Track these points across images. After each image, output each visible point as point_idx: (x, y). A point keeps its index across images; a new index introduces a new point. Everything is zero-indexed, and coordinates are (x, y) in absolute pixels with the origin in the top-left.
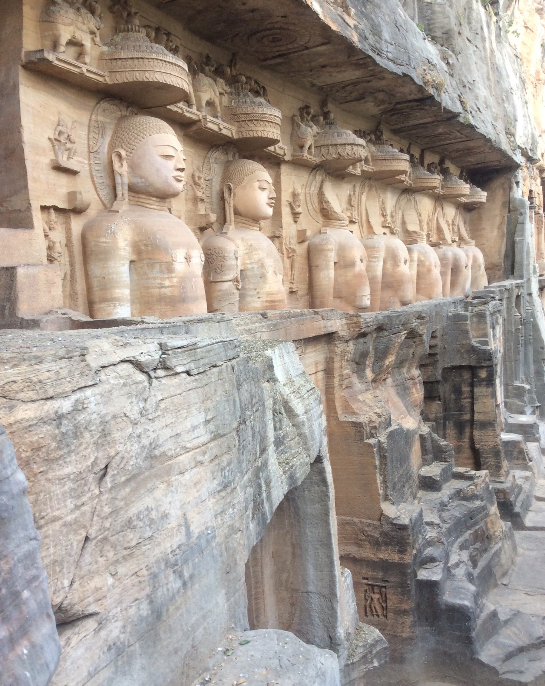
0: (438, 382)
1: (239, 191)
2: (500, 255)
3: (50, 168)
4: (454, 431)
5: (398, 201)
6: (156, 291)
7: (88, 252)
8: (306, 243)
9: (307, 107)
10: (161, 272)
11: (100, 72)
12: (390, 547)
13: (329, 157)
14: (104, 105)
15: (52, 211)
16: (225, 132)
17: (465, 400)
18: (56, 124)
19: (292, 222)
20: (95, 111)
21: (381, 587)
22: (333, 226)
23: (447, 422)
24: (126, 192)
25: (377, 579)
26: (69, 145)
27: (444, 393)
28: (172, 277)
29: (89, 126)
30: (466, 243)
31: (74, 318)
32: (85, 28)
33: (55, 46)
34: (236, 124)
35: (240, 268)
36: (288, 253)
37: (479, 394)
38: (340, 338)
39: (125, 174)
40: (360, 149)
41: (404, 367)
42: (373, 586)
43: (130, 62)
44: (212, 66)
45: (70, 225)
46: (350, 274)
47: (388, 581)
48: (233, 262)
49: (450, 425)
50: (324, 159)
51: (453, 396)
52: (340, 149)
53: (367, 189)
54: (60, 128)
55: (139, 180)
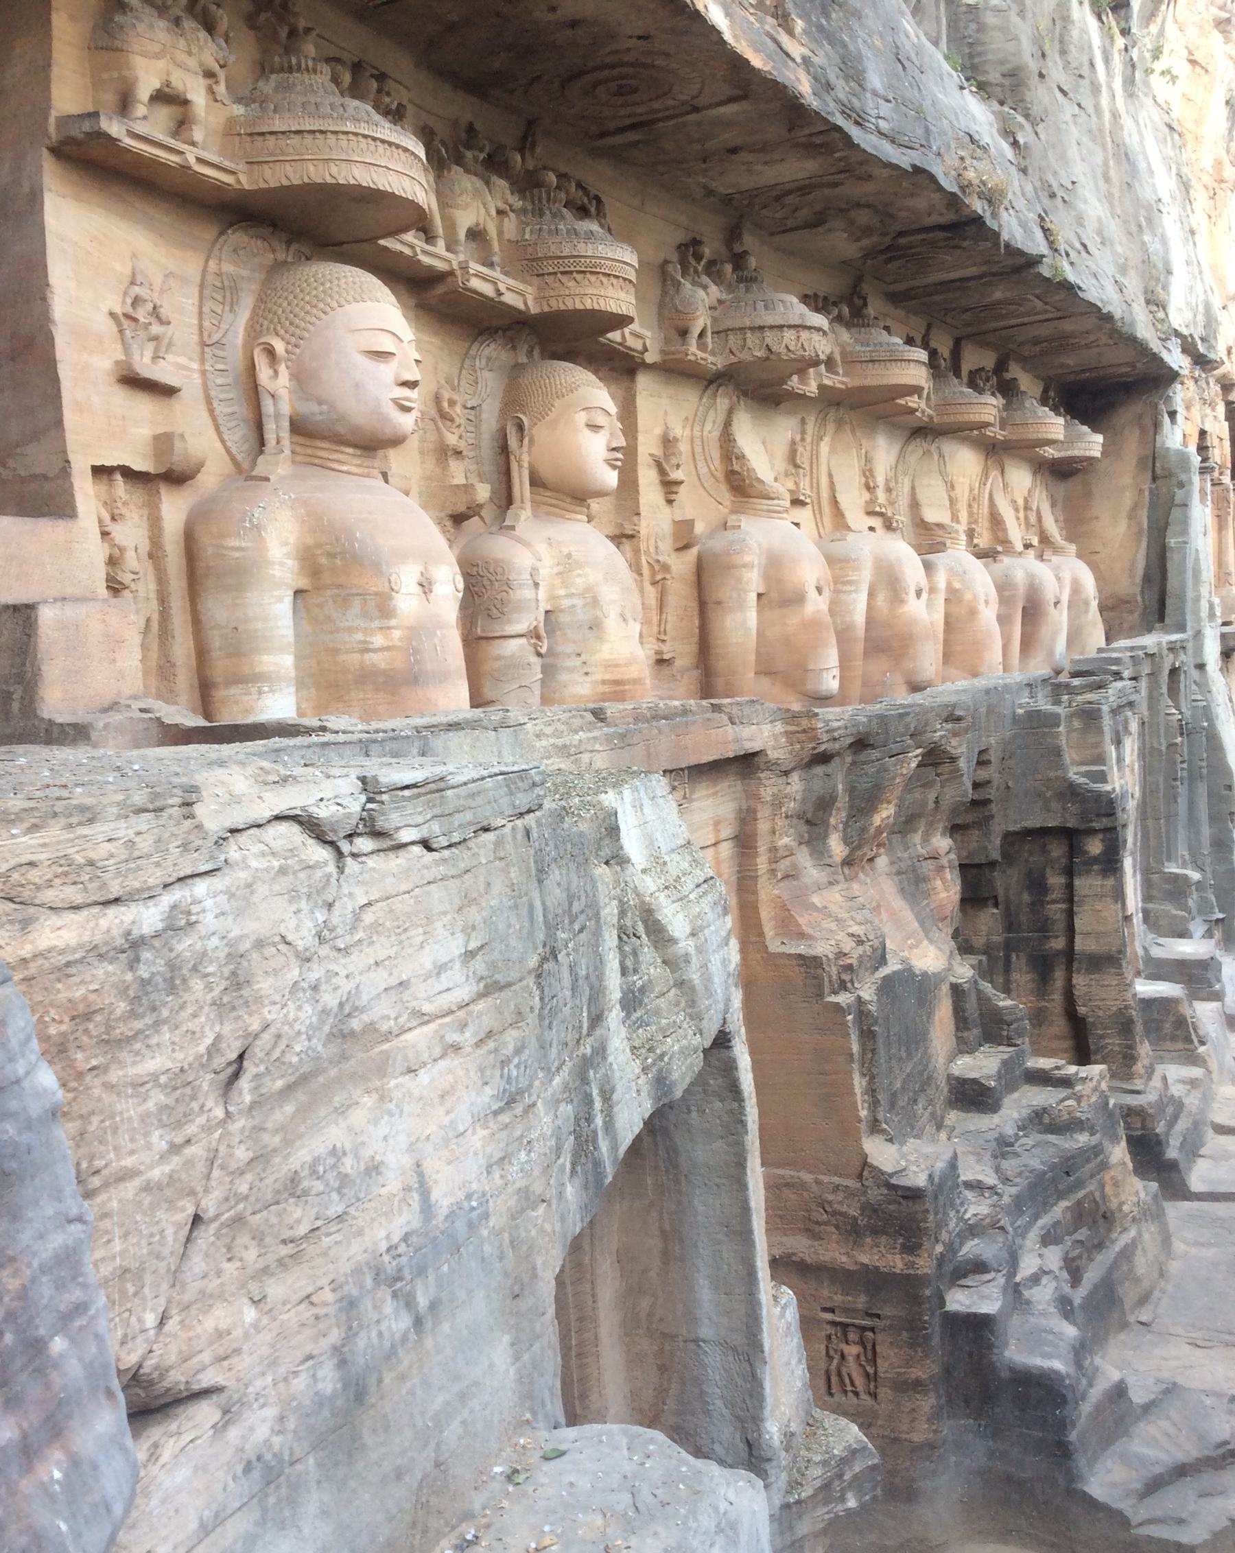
0: (992, 864)
1: (541, 433)
2: (1132, 576)
3: (113, 380)
4: (1029, 977)
5: (902, 454)
6: (353, 659)
7: (199, 572)
8: (694, 551)
9: (696, 242)
10: (365, 615)
11: (227, 164)
12: (883, 1239)
13: (745, 356)
14: (237, 237)
15: (118, 477)
16: (509, 299)
17: (1053, 906)
18: (127, 280)
19: (662, 502)
20: (216, 251)
21: (863, 1329)
22: (755, 512)
23: (1014, 956)
24: (285, 434)
25: (855, 1310)
26: (156, 329)
27: (1007, 889)
28: (389, 628)
29: (202, 286)
30: (1057, 550)
31: (167, 721)
32: (192, 62)
33: (124, 104)
34: (536, 280)
35: (544, 606)
36: (653, 572)
37: (1086, 892)
38: (771, 766)
39: (283, 393)
40: (816, 337)
41: (915, 831)
42: (845, 1326)
43: (295, 141)
44: (481, 151)
45: (159, 510)
46: (792, 621)
47: (878, 1316)
48: (528, 594)
49: (1019, 961)
50: (733, 359)
51: (1026, 897)
52: (770, 337)
53: (831, 427)
54: (136, 290)
55: (315, 408)
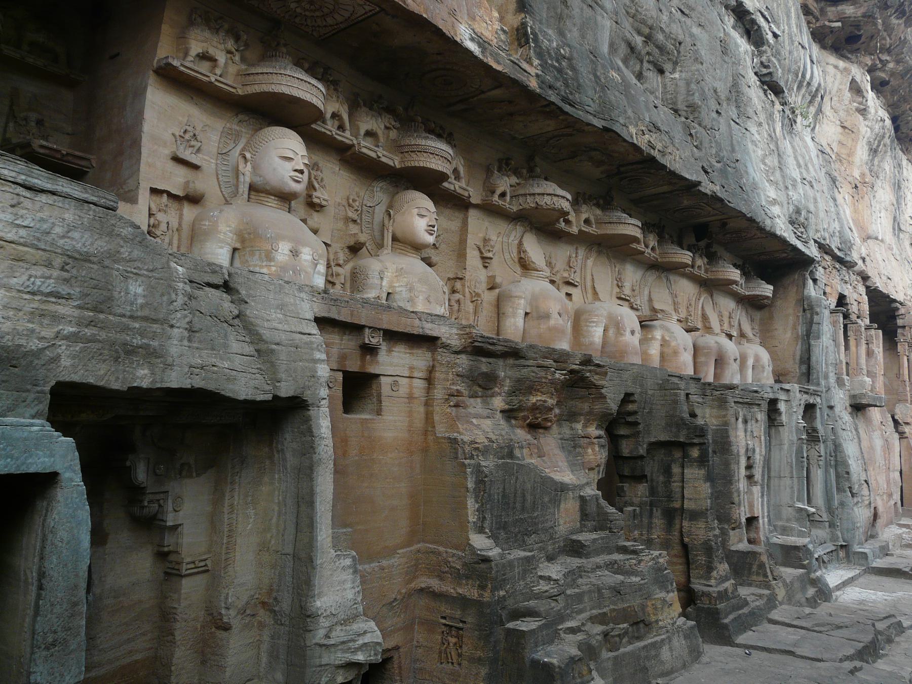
0: (642, 457)
1: (398, 218)
2: (794, 359)
4: (662, 521)
5: (643, 276)
8: (497, 291)
9: (508, 159)
10: (260, 259)
11: (235, 85)
12: (470, 582)
13: (526, 206)
15: (165, 195)
16: (384, 159)
17: (675, 484)
22: (532, 277)
23: (655, 509)
24: (246, 190)
25: (455, 618)
26: (193, 143)
27: (652, 473)
30: (749, 341)
34: (401, 155)
35: (385, 289)
37: (690, 476)
38: (445, 346)
42: (451, 626)
43: (261, 76)
44: (706, 271)
46: (543, 327)
47: (465, 622)
49: (657, 513)
51: (661, 479)
52: (538, 199)
55: (258, 179)
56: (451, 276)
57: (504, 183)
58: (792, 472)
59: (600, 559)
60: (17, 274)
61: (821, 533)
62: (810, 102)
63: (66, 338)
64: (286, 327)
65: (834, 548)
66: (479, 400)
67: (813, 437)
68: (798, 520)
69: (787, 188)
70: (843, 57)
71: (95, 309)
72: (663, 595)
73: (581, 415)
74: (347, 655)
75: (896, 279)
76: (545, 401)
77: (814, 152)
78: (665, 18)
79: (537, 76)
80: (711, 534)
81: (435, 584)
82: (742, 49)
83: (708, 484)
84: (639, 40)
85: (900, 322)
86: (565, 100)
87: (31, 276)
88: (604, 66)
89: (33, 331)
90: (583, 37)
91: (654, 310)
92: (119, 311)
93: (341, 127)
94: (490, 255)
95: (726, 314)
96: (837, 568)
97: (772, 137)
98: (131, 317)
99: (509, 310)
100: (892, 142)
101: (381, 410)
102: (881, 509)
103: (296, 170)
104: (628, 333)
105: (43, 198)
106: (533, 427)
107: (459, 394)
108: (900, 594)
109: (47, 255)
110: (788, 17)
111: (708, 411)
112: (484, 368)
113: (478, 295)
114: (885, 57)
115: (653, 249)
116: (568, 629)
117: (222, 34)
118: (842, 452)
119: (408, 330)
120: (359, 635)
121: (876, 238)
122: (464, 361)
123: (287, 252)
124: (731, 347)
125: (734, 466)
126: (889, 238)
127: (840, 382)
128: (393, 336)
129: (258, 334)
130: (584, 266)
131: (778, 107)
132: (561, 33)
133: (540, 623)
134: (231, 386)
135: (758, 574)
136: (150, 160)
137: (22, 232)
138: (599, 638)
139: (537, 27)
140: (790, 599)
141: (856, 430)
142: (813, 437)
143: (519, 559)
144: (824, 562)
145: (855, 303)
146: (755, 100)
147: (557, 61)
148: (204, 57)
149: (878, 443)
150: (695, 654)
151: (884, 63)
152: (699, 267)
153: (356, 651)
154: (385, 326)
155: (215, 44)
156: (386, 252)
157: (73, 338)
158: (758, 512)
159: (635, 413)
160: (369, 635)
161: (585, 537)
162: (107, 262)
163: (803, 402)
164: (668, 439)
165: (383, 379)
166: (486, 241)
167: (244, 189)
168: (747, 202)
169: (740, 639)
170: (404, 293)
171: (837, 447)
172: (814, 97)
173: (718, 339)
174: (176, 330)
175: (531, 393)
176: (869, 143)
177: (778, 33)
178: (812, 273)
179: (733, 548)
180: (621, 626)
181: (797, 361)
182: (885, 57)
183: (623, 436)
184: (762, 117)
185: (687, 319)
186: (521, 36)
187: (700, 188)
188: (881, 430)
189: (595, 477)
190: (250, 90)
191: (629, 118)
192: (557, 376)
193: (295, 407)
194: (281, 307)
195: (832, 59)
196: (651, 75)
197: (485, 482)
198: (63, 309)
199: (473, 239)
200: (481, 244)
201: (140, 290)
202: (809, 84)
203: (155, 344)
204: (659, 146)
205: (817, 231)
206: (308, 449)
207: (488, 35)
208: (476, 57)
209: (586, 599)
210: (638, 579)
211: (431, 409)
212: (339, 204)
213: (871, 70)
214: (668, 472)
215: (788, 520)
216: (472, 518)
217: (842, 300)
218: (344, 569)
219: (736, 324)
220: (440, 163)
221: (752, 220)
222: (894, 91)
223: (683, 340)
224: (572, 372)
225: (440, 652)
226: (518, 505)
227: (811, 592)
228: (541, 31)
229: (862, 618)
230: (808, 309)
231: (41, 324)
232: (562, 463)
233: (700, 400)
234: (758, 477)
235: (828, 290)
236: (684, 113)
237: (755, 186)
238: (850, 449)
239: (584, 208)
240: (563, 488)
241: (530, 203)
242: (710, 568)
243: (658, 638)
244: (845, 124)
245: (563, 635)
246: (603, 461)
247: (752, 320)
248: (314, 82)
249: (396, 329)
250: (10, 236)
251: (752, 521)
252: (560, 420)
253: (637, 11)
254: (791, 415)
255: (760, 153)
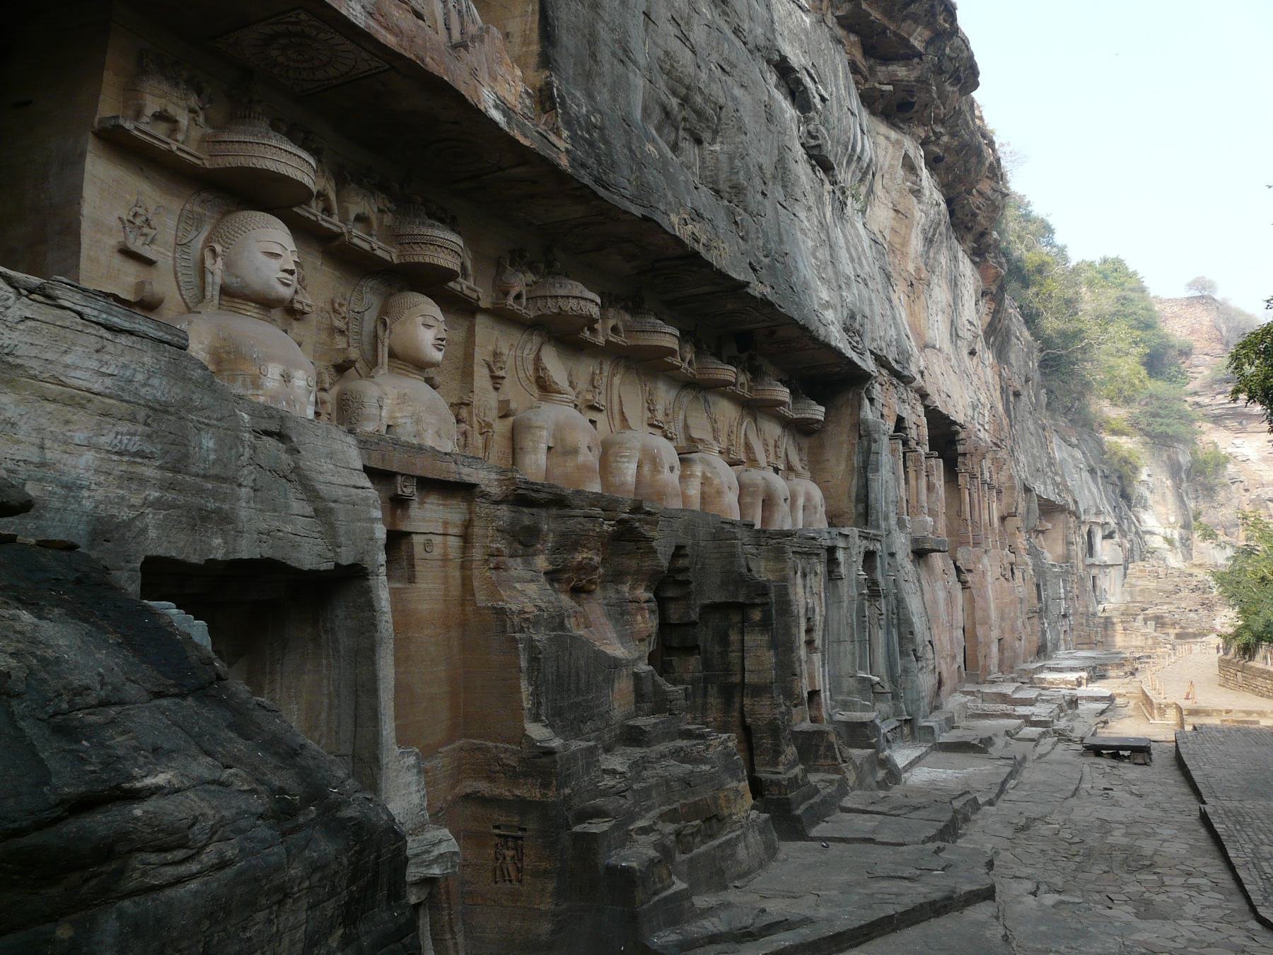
0: (694, 624)
1: (397, 328)
8: (511, 419)
10: (244, 385)
16: (379, 253)
17: (734, 654)
19: (491, 388)
21: (517, 838)
24: (216, 293)
26: (146, 230)
29: (180, 216)
30: (798, 475)
32: (183, 103)
33: (138, 114)
35: (385, 422)
36: (481, 427)
38: (485, 495)
39: (218, 272)
40: (593, 305)
41: (625, 583)
42: (506, 837)
44: (750, 389)
46: (570, 464)
47: (524, 830)
48: (375, 411)
49: (713, 690)
51: (717, 648)
52: (561, 302)
55: (234, 280)
56: (455, 401)
57: (520, 282)
58: (852, 635)
59: (663, 747)
60: (105, 432)
61: (885, 707)
62: (861, 180)
63: (152, 505)
64: (340, 481)
65: (897, 724)
66: (519, 560)
67: (874, 592)
68: (860, 692)
69: (840, 287)
70: (893, 126)
71: (175, 470)
72: (734, 784)
73: (628, 574)
74: (421, 870)
75: (955, 396)
76: (591, 559)
77: (866, 242)
78: (704, 76)
79: (567, 151)
80: (777, 711)
81: (483, 787)
82: (788, 116)
83: (772, 652)
84: (674, 102)
85: (960, 449)
86: (598, 181)
87: (117, 434)
88: (639, 137)
89: (123, 498)
90: (614, 100)
91: (690, 439)
92: (194, 469)
93: (327, 210)
94: (502, 373)
95: (771, 442)
96: (901, 748)
97: (822, 225)
98: (204, 476)
99: (528, 444)
100: (948, 229)
101: (414, 577)
102: (945, 675)
103: (285, 271)
104: (666, 469)
105: (123, 340)
106: (577, 591)
107: (499, 553)
108: (971, 769)
109: (131, 407)
110: (836, 76)
111: (763, 563)
112: (527, 521)
113: (489, 425)
114: (939, 129)
115: (690, 363)
116: (641, 828)
117: (183, 86)
118: (905, 608)
119: (443, 476)
120: (434, 845)
121: (934, 347)
122: (504, 512)
123: (277, 376)
124: (779, 483)
125: (794, 630)
126: (947, 346)
127: (901, 524)
128: (429, 485)
129: (314, 490)
130: (610, 385)
131: (828, 187)
132: (590, 96)
133: (611, 824)
134: (296, 555)
135: (826, 757)
136: (92, 253)
137: (108, 382)
138: (672, 837)
139: (563, 88)
140: (861, 784)
141: (919, 581)
142: (874, 592)
143: (582, 750)
144: (888, 741)
145: (914, 427)
146: (804, 179)
147: (588, 132)
148: (161, 117)
149: (941, 595)
150: (772, 852)
151: (938, 136)
152: (742, 384)
153: (431, 864)
154: (419, 473)
155: (175, 100)
156: (381, 372)
157: (157, 504)
158: (819, 685)
159: (686, 569)
160: (444, 844)
161: (641, 722)
162: (183, 413)
163: (862, 550)
164: (724, 599)
165: (414, 536)
166: (496, 355)
167: (213, 292)
168: (800, 306)
169: (814, 832)
170: (408, 426)
171: (900, 602)
172: (865, 174)
173: (763, 473)
174: (243, 489)
175: (576, 550)
176: (924, 231)
177: (827, 96)
178: (868, 392)
179: (796, 729)
180: (694, 823)
181: (853, 499)
182: (939, 129)
183: (672, 599)
184: (812, 200)
185: (729, 450)
186: (545, 99)
187: (749, 291)
188: (943, 580)
189: (646, 649)
190: (221, 163)
191: (670, 203)
192: (605, 527)
193: (355, 575)
194: (331, 455)
195: (883, 128)
196: (686, 145)
197: (539, 659)
198: (150, 471)
199: (481, 354)
200: (490, 360)
201: (211, 444)
202: (859, 158)
203: (226, 507)
204: (703, 239)
205: (873, 340)
206: (368, 625)
207: (511, 99)
208: (501, 129)
209: (654, 794)
210: (707, 767)
211: (468, 573)
212: (322, 310)
213: (924, 143)
214: (724, 641)
215: (850, 693)
216: (527, 704)
217: (900, 423)
218: (408, 769)
219: (783, 455)
220: (449, 258)
221: (804, 329)
222: (949, 169)
223: (726, 476)
224: (621, 522)
225: (495, 870)
226: (573, 687)
227: (881, 774)
228: (569, 93)
229: (932, 798)
230: (864, 434)
231: (129, 489)
232: (612, 635)
233: (755, 551)
234: (818, 642)
235: (886, 411)
236: (726, 195)
237: (806, 285)
238: (914, 604)
239: (611, 312)
240: (616, 664)
241: (552, 307)
242: (777, 752)
243: (733, 835)
244: (899, 208)
245: (635, 836)
246: (654, 630)
247: (800, 450)
248: (305, 155)
249: (430, 476)
250: (97, 387)
251: (814, 694)
252: (605, 581)
253: (672, 66)
254: (851, 567)
255: (810, 244)
